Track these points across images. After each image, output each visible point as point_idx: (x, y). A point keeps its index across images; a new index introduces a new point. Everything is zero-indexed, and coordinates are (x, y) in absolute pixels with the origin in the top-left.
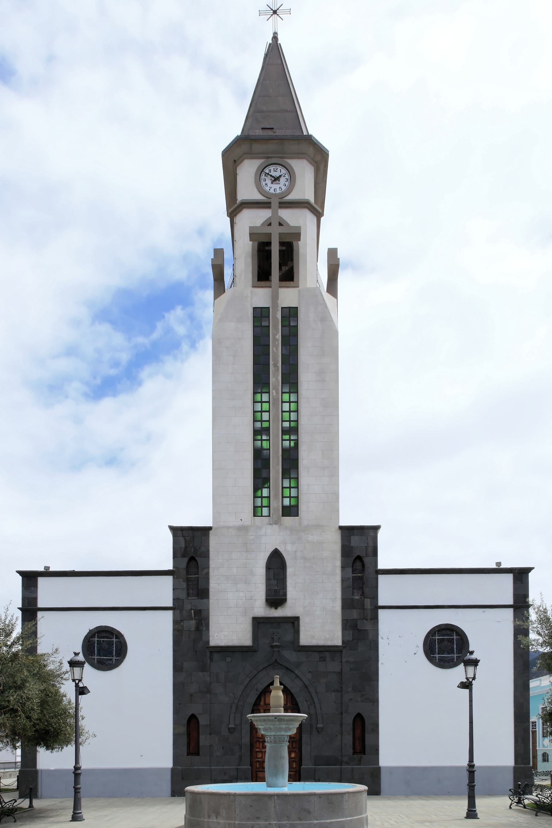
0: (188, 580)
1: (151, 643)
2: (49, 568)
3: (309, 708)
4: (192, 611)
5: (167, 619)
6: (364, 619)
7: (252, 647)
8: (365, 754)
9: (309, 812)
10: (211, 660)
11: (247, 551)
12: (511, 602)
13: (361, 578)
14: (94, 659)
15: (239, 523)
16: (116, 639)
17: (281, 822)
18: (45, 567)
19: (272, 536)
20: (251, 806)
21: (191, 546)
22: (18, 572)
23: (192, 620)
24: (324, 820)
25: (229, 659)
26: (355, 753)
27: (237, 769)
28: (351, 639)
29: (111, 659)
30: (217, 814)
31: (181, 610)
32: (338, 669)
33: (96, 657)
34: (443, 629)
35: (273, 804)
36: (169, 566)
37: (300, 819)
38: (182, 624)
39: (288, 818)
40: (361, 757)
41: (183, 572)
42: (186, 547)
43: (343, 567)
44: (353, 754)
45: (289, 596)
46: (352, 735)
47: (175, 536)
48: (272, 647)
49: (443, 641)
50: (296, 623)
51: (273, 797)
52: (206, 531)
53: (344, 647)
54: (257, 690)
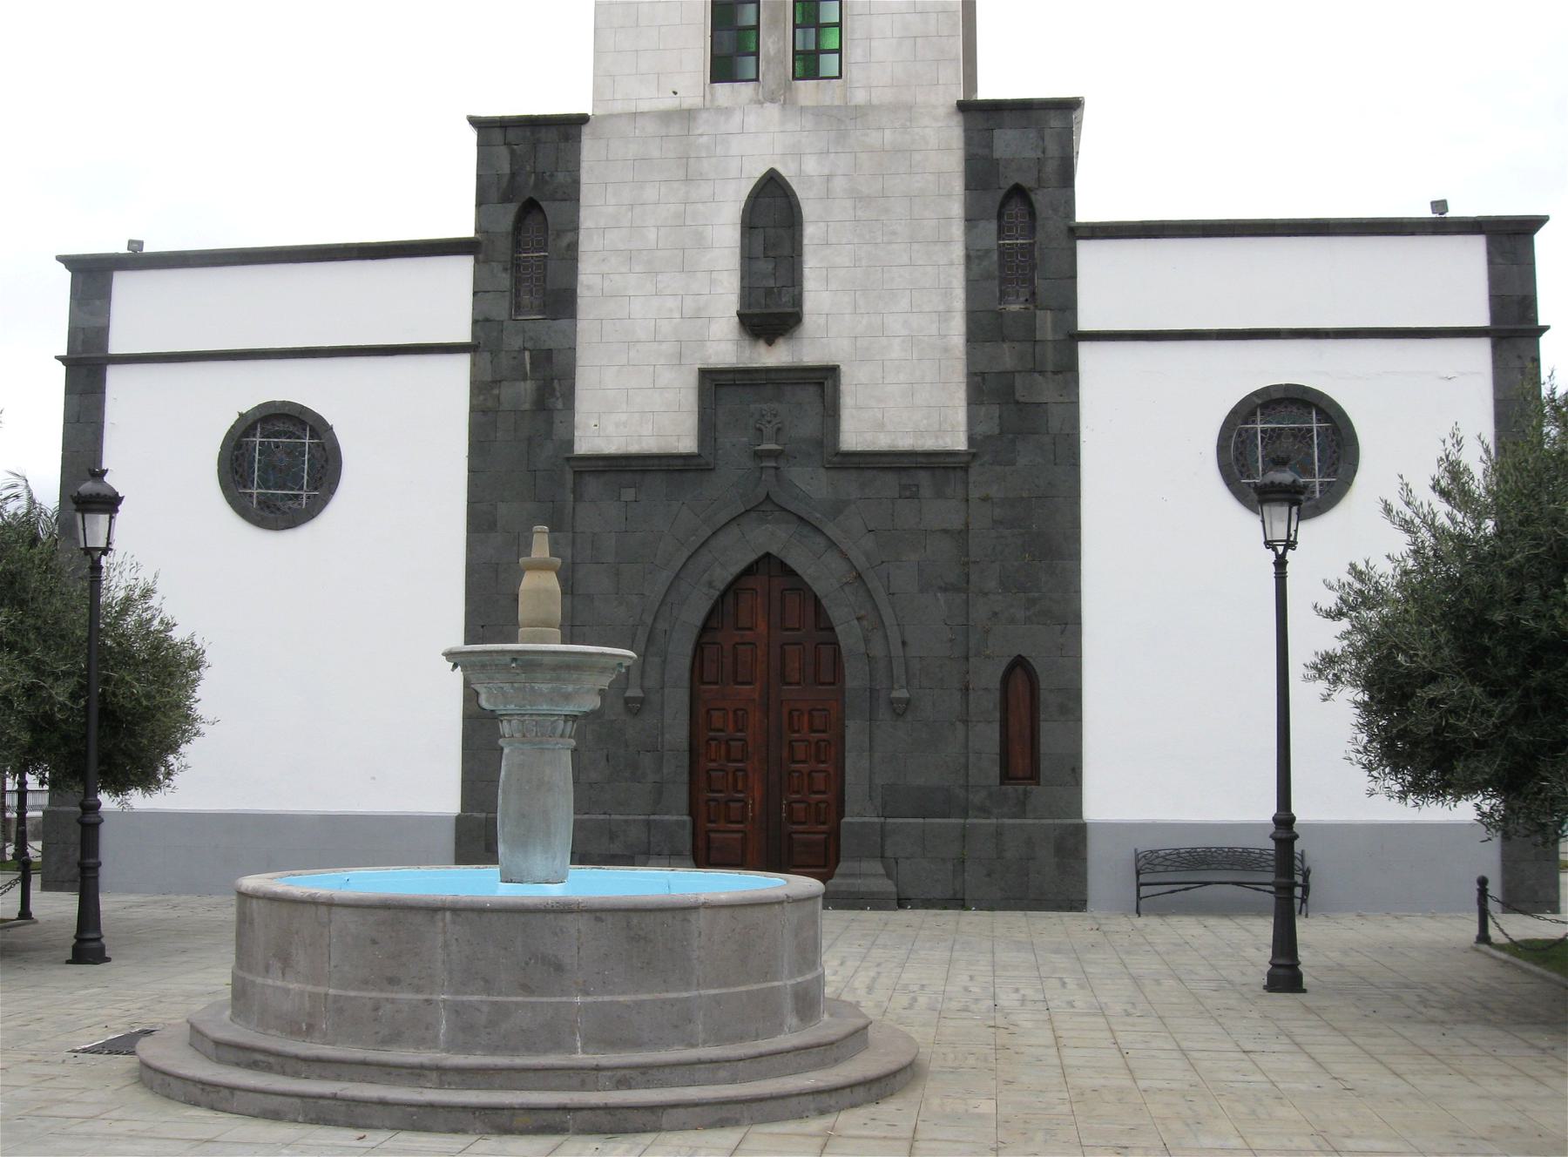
0: (516, 266)
1: (410, 448)
2: (141, 243)
3: (867, 640)
4: (527, 354)
5: (453, 380)
6: (1033, 370)
7: (699, 456)
8: (1038, 784)
9: (559, 968)
10: (578, 497)
11: (687, 180)
12: (1482, 319)
13: (1028, 251)
14: (251, 495)
15: (669, 103)
16: (312, 437)
17: (465, 998)
18: (131, 242)
19: (760, 133)
20: (374, 942)
21: (530, 170)
22: (60, 259)
23: (525, 379)
24: (611, 993)
25: (629, 494)
26: (1006, 776)
27: (648, 823)
28: (997, 431)
29: (297, 496)
30: (286, 961)
31: (495, 353)
32: (956, 523)
33: (255, 491)
34: (1279, 401)
35: (440, 939)
36: (464, 226)
37: (526, 989)
38: (496, 392)
39: (488, 985)
40: (1025, 793)
41: (504, 246)
42: (513, 175)
43: (971, 220)
44: (1002, 783)
45: (809, 305)
46: (997, 726)
47: (482, 145)
48: (759, 455)
49: (1279, 436)
50: (829, 384)
51: (439, 916)
52: (569, 127)
53: (974, 455)
54: (710, 584)
